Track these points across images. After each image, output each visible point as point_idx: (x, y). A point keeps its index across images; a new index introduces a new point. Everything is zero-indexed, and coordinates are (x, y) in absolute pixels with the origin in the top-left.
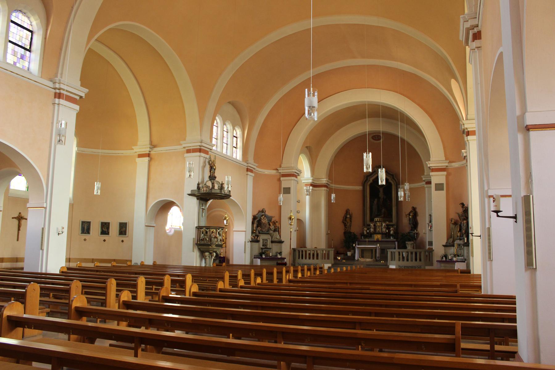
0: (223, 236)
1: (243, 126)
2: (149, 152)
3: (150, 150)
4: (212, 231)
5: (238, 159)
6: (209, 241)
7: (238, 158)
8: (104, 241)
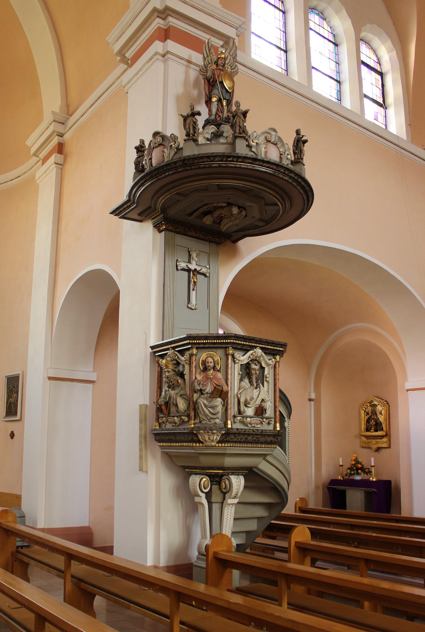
0: (381, 413)
1: (397, 30)
2: (60, 138)
3: (60, 129)
4: (204, 363)
5: (395, 133)
6: (188, 416)
7: (393, 129)
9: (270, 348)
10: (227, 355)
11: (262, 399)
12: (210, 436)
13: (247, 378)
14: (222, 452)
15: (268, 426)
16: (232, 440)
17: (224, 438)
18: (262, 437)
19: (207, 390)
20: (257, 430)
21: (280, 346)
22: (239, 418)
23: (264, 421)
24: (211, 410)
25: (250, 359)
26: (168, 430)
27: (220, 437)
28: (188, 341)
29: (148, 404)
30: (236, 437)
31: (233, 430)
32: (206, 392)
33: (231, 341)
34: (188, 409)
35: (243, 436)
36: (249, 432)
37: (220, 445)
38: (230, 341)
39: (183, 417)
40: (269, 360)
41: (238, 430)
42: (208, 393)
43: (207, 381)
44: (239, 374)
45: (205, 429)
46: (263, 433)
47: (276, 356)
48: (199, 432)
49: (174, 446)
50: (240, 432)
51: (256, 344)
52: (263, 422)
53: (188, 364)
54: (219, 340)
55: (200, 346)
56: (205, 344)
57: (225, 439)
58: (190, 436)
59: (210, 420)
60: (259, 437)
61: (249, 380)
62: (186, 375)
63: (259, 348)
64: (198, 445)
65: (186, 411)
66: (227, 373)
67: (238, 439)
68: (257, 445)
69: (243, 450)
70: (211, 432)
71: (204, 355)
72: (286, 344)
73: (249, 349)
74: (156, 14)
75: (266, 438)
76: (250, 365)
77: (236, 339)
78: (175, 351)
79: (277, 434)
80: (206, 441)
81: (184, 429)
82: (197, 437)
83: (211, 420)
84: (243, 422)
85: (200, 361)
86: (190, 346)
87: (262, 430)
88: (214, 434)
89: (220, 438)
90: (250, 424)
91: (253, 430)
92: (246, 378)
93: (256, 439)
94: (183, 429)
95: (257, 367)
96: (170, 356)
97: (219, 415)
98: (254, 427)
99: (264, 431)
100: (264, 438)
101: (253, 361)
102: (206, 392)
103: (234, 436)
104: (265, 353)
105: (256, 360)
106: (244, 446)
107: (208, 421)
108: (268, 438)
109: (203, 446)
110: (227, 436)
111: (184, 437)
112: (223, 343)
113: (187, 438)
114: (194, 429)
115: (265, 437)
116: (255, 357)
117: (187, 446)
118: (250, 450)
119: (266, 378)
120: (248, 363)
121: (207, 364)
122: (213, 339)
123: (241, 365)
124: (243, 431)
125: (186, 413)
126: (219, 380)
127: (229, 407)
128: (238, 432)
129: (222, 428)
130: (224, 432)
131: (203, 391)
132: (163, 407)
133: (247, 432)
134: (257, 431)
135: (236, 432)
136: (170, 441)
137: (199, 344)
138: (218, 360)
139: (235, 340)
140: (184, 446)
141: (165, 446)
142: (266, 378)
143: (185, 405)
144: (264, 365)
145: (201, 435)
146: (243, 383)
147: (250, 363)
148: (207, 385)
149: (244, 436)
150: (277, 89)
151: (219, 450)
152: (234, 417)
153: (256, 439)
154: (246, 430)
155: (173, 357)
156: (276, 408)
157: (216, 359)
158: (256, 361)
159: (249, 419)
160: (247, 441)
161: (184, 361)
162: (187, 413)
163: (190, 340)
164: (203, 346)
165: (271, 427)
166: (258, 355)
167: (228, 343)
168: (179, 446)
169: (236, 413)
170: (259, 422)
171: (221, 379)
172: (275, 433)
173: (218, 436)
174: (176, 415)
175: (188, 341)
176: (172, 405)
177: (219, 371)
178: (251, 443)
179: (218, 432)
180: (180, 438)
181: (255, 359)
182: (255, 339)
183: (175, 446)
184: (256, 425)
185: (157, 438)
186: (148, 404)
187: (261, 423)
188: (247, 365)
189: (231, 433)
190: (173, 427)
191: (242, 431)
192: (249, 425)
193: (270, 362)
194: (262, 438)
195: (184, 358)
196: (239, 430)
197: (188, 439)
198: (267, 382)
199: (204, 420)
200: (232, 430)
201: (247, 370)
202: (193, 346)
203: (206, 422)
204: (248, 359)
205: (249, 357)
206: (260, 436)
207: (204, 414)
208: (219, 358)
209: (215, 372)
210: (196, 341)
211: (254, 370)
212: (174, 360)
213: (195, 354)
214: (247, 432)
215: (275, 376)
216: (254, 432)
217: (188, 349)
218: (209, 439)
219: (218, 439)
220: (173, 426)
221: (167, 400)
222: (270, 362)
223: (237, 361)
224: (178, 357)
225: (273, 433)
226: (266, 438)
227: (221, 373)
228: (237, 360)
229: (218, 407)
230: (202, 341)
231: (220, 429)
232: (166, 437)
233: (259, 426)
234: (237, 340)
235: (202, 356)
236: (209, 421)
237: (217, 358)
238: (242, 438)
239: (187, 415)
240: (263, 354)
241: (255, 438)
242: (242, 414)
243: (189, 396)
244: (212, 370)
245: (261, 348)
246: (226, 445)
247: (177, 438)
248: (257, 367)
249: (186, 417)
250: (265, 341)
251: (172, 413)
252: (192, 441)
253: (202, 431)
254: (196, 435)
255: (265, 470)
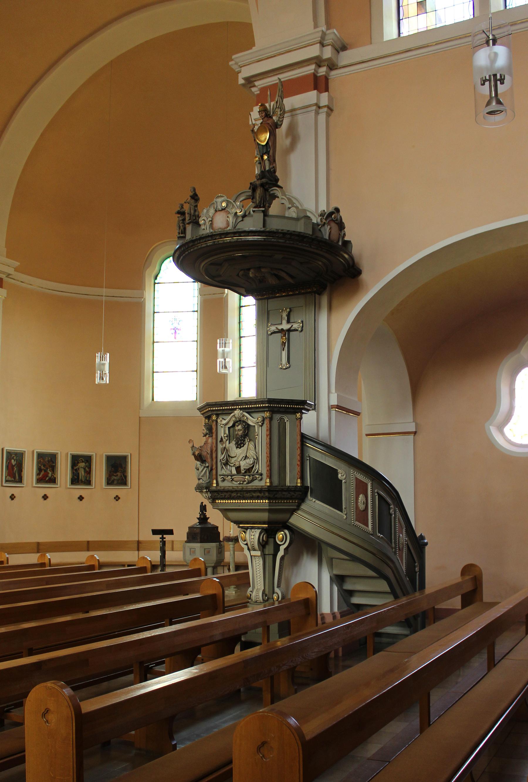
8: (45, 497)
14: (235, 507)
15: (259, 482)
18: (247, 493)
35: (226, 493)
60: (243, 494)
69: (286, 506)
74: (324, 45)
79: (259, 489)
103: (217, 494)
106: (244, 502)
115: (250, 493)
150: (385, 64)
153: (241, 495)
214: (226, 489)
226: (251, 493)
231: (201, 488)
255: (301, 527)
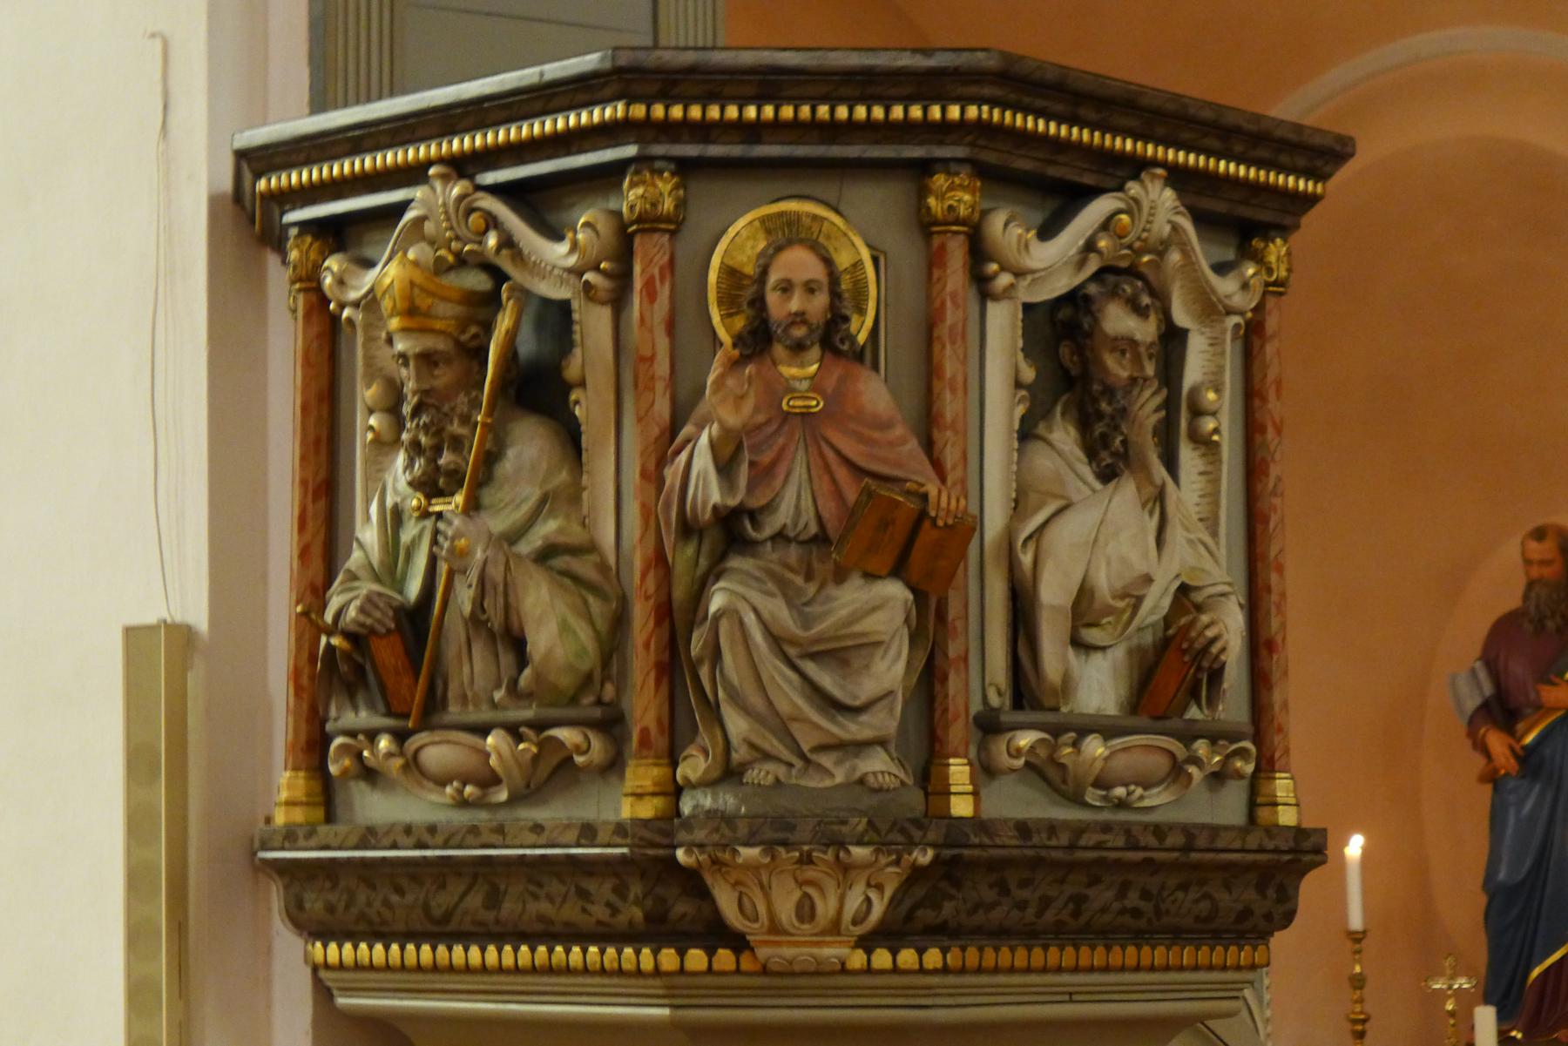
6: (611, 723)
9: (1246, 178)
10: (927, 226)
11: (1177, 584)
12: (811, 891)
13: (1063, 414)
16: (979, 918)
17: (916, 907)
18: (1184, 887)
19: (782, 516)
20: (1159, 830)
21: (1301, 162)
22: (1025, 739)
23: (1196, 761)
24: (826, 679)
25: (1093, 265)
26: (427, 838)
27: (888, 893)
28: (613, 111)
29: (198, 615)
30: (1004, 890)
31: (990, 835)
32: (771, 526)
33: (972, 112)
34: (606, 661)
36: (1098, 846)
37: (882, 958)
38: (963, 112)
39: (565, 734)
40: (1221, 269)
41: (1030, 838)
42: (788, 540)
43: (781, 441)
44: (1018, 385)
45: (780, 835)
46: (1194, 856)
47: (1268, 239)
48: (727, 856)
49: (468, 969)
50: (1043, 853)
51: (1146, 139)
52: (1192, 769)
53: (602, 295)
54: (869, 101)
55: (715, 150)
56: (753, 132)
57: (926, 916)
58: (636, 889)
59: (814, 757)
61: (1084, 425)
62: (582, 384)
63: (1160, 171)
64: (696, 958)
65: (587, 680)
66: (930, 372)
67: (1022, 906)
68: (1146, 949)
70: (829, 856)
71: (741, 223)
72: (1349, 149)
73: (1088, 179)
75: (1206, 896)
76: (1090, 312)
77: (1013, 97)
78: (479, 188)
79: (1287, 857)
80: (775, 928)
81: (588, 833)
82: (704, 894)
83: (826, 760)
84: (1052, 773)
85: (713, 277)
86: (630, 151)
87: (1189, 831)
88: (853, 874)
89: (894, 902)
90: (1098, 784)
91: (1127, 829)
92: (1059, 409)
93: (1143, 905)
94: (571, 836)
95: (1145, 331)
96: (429, 227)
97: (884, 721)
98: (1122, 805)
99: (1202, 841)
100: (1194, 894)
101: (1111, 278)
102: (771, 526)
103: (991, 886)
104: (1202, 220)
105: (1133, 272)
107: (798, 763)
108: (1224, 898)
109: (738, 971)
110: (944, 885)
111: (583, 894)
112: (906, 131)
113: (608, 905)
114: (682, 836)
116: (1130, 247)
117: (603, 971)
118: (1096, 996)
119: (1197, 412)
120: (1074, 298)
121: (772, 298)
122: (908, 90)
123: (1027, 308)
124: (1064, 839)
125: (588, 700)
126: (876, 435)
127: (954, 649)
128: (1030, 853)
129: (916, 823)
130: (925, 857)
131: (748, 526)
132: (388, 654)
133: (1085, 848)
134: (1152, 841)
135: (1016, 852)
136: (441, 931)
137: (703, 132)
138: (857, 265)
139: (1004, 106)
140: (568, 970)
141: (388, 967)
142: (1197, 412)
143: (584, 634)
144: (1181, 317)
145: (736, 884)
146: (1043, 461)
147: (1087, 299)
148: (781, 470)
149: (1062, 881)
151: (843, 1001)
152: (989, 726)
153: (1143, 905)
154: (1080, 830)
155: (457, 238)
156: (1264, 652)
157: (843, 260)
158: (1140, 284)
159: (1095, 748)
160: (1083, 919)
161: (570, 271)
162: (599, 702)
163: (631, 99)
164: (735, 150)
165: (1229, 808)
166: (1155, 227)
167: (944, 130)
168: (517, 970)
169: (1000, 693)
170: (1160, 763)
171: (885, 425)
172: (1276, 851)
173: (880, 888)
174: (500, 716)
175: (613, 111)
176: (455, 630)
177: (858, 356)
178: (1106, 935)
179: (883, 860)
180: (544, 907)
181: (1124, 264)
182: (1145, 101)
183: (484, 969)
184: (1139, 791)
185: (315, 903)
186: (198, 615)
187: (1177, 772)
188: (1065, 313)
189: (974, 864)
190: (462, 818)
191: (1054, 842)
192: (1092, 796)
193: (1226, 286)
194: (1180, 895)
195: (563, 248)
196: (1036, 840)
197: (615, 911)
198: (1206, 444)
199: (767, 756)
200: (986, 841)
201: (1065, 351)
202: (658, 149)
203: (781, 771)
204: (1081, 264)
205: (1090, 247)
206: (1172, 882)
207: (770, 703)
208: (865, 254)
209: (837, 370)
210: (677, 112)
211: (1123, 352)
212: (462, 262)
213: (668, 220)
214: (1085, 848)
215: (1257, 402)
216: (1135, 847)
217: (608, 177)
218: (806, 911)
219: (878, 910)
220: (462, 803)
221: (414, 588)
222: (1226, 286)
223: (1005, 280)
224: (508, 242)
225: (1261, 850)
227: (875, 367)
228: (1003, 269)
229: (880, 651)
230: (732, 112)
231: (903, 831)
232: (395, 898)
233: (1157, 797)
234: (1016, 108)
235: (724, 232)
236: (807, 761)
237: (853, 251)
238: (1046, 903)
239: (597, 713)
240: (1186, 224)
241: (1133, 899)
242: (1048, 702)
243: (612, 560)
244: (815, 352)
245: (1179, 177)
246: (933, 958)
247: (509, 907)
248: (1145, 331)
249: (591, 735)
250: (1207, 114)
251: (464, 700)
252: (656, 931)
253: (749, 853)
254: (693, 883)
